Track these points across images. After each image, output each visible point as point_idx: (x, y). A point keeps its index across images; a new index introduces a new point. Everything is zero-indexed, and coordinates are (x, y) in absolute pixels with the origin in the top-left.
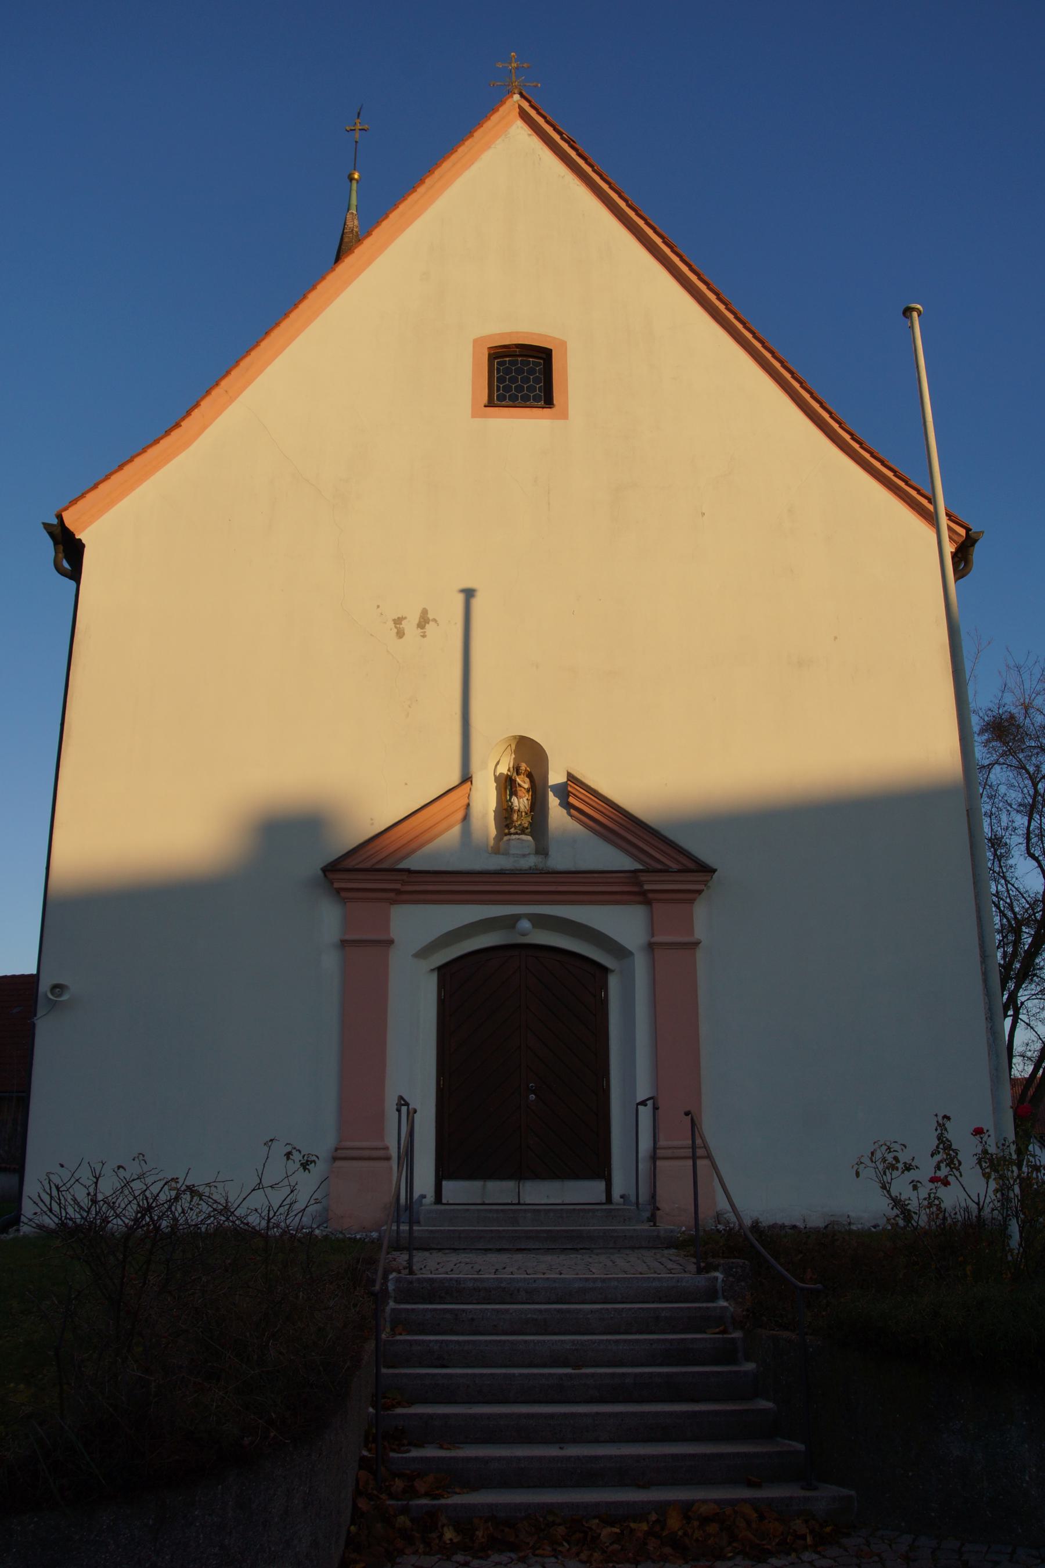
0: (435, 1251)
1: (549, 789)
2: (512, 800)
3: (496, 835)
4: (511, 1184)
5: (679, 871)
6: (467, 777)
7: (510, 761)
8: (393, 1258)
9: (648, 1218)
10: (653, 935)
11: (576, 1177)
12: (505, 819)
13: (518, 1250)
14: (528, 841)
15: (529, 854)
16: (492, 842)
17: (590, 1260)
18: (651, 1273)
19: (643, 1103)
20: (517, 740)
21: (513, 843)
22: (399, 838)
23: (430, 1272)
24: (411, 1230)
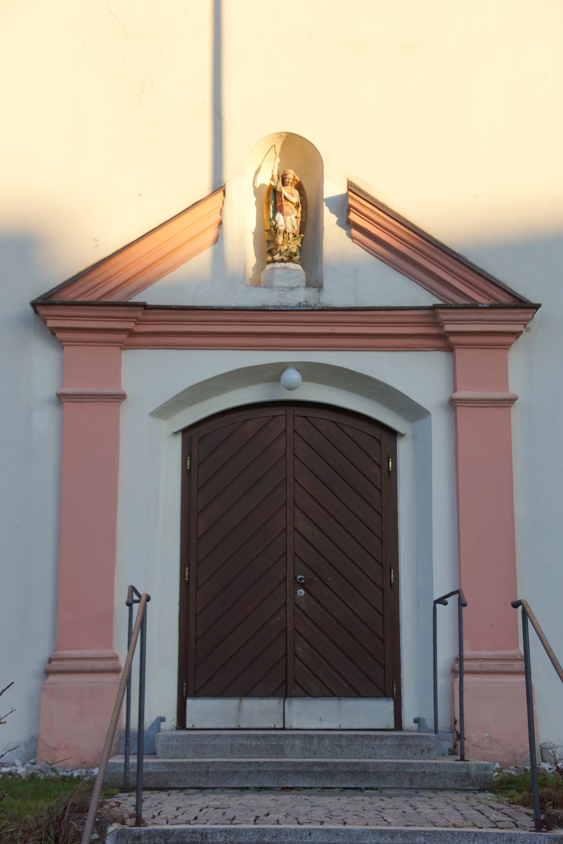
0: (174, 792)
1: (324, 203)
2: (277, 218)
3: (256, 264)
4: (273, 703)
5: (491, 307)
6: (219, 187)
7: (274, 167)
8: (116, 802)
9: (449, 750)
10: (455, 390)
11: (358, 694)
12: (267, 243)
13: (284, 789)
14: (297, 270)
15: (298, 287)
16: (250, 273)
17: (383, 804)
18: (469, 826)
19: (442, 601)
20: (283, 139)
21: (277, 272)
22: (131, 264)
23: (165, 821)
24: (140, 764)
